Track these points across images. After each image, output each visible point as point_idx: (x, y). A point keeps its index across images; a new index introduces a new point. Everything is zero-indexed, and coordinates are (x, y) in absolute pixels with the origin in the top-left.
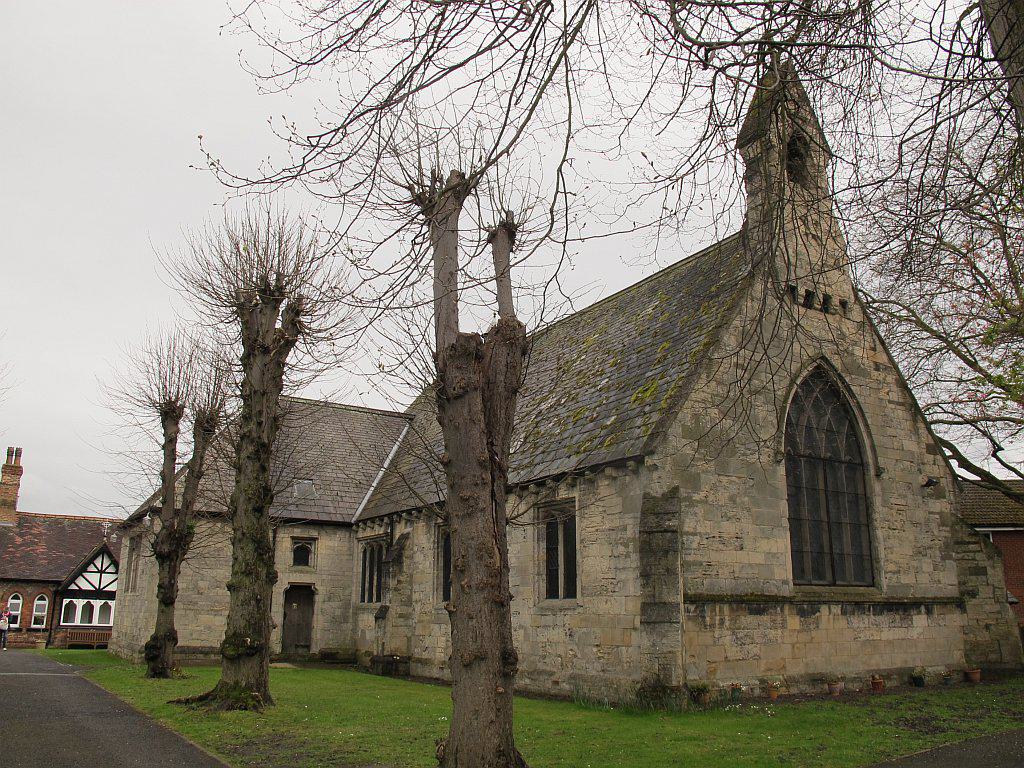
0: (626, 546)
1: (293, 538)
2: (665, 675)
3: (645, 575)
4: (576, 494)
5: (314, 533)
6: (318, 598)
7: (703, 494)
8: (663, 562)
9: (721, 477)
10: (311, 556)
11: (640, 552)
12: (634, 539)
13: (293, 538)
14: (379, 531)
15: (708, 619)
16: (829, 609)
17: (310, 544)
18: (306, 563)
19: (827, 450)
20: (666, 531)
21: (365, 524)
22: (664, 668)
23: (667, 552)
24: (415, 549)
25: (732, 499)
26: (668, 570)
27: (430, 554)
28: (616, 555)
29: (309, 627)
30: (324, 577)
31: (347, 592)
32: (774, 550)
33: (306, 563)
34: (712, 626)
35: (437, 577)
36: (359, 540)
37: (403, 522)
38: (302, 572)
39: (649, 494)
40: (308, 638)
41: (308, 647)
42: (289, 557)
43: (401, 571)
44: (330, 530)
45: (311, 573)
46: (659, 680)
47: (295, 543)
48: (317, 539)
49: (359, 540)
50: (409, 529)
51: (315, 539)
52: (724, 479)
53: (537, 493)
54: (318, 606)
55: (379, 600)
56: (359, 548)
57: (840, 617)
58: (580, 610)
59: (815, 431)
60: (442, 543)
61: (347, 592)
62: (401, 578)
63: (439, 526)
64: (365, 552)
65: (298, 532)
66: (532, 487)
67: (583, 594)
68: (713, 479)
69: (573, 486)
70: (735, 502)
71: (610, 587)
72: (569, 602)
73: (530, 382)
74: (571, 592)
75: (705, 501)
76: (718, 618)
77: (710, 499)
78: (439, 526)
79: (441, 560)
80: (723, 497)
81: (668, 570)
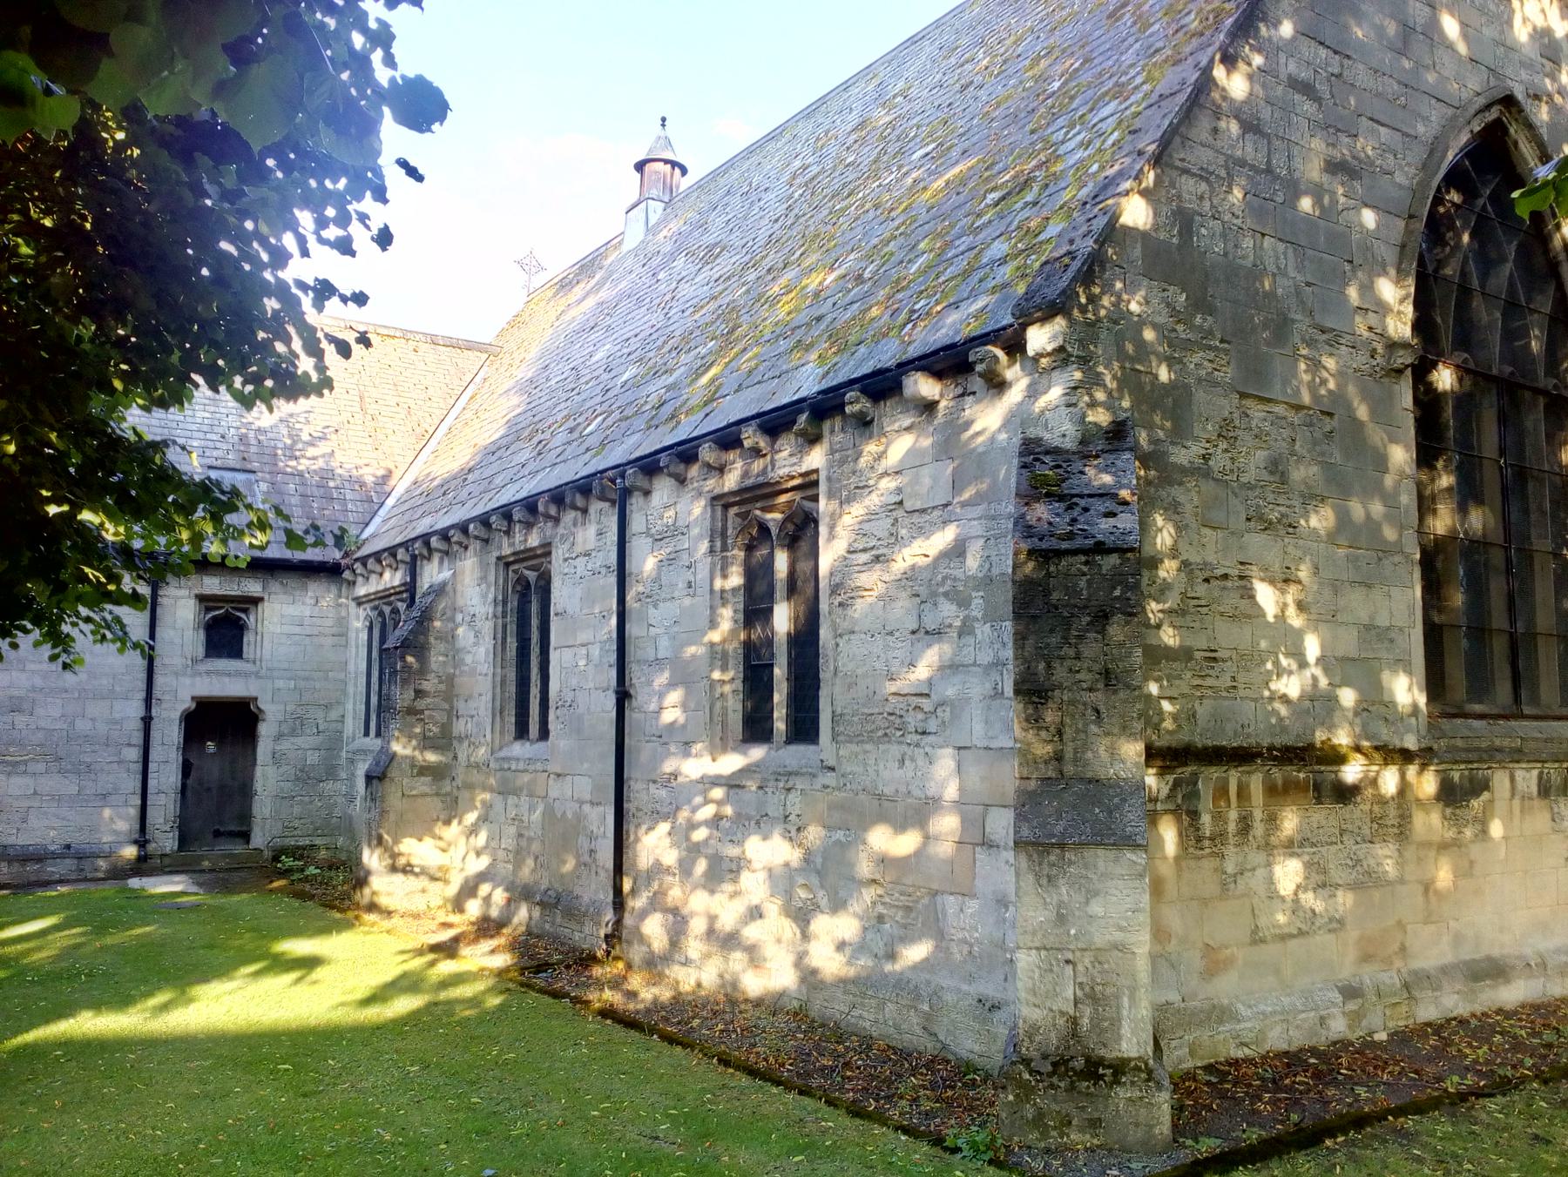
0: (963, 603)
1: (202, 598)
2: (1096, 1022)
3: (1033, 691)
4: (816, 458)
5: (252, 587)
6: (265, 730)
7: (1196, 449)
8: (1091, 649)
9: (1248, 402)
10: (248, 638)
11: (1017, 616)
12: (987, 582)
13: (202, 598)
14: (392, 578)
15: (1206, 819)
16: (1512, 779)
17: (245, 611)
18: (237, 653)
19: (1503, 360)
20: (1100, 548)
21: (379, 561)
22: (1092, 996)
23: (1102, 618)
24: (459, 617)
25: (1276, 468)
26: (1107, 675)
27: (487, 628)
28: (931, 627)
29: (245, 791)
30: (280, 684)
31: (334, 715)
32: (1383, 621)
33: (237, 653)
34: (1219, 837)
35: (503, 682)
36: (359, 602)
37: (436, 557)
38: (218, 673)
39: (1038, 441)
40: (246, 817)
41: (245, 836)
42: (194, 641)
43: (423, 671)
44: (292, 582)
45: (246, 675)
46: (1074, 1035)
47: (208, 610)
48: (261, 599)
49: (359, 602)
50: (446, 574)
51: (256, 601)
52: (1257, 412)
53: (721, 470)
54: (264, 748)
55: (378, 734)
56: (358, 621)
57: (1537, 803)
58: (829, 779)
59: (1477, 302)
60: (513, 603)
61: (334, 715)
62: (426, 686)
63: (507, 565)
64: (371, 629)
65: (213, 585)
66: (707, 453)
67: (835, 737)
68: (1226, 405)
69: (813, 440)
70: (1284, 479)
71: (913, 720)
72: (798, 754)
73: (1190, 1159)
74: (804, 728)
75: (1202, 470)
76: (1233, 815)
77: (1219, 461)
78: (507, 565)
79: (512, 643)
80: (1254, 462)
81: (1107, 675)
